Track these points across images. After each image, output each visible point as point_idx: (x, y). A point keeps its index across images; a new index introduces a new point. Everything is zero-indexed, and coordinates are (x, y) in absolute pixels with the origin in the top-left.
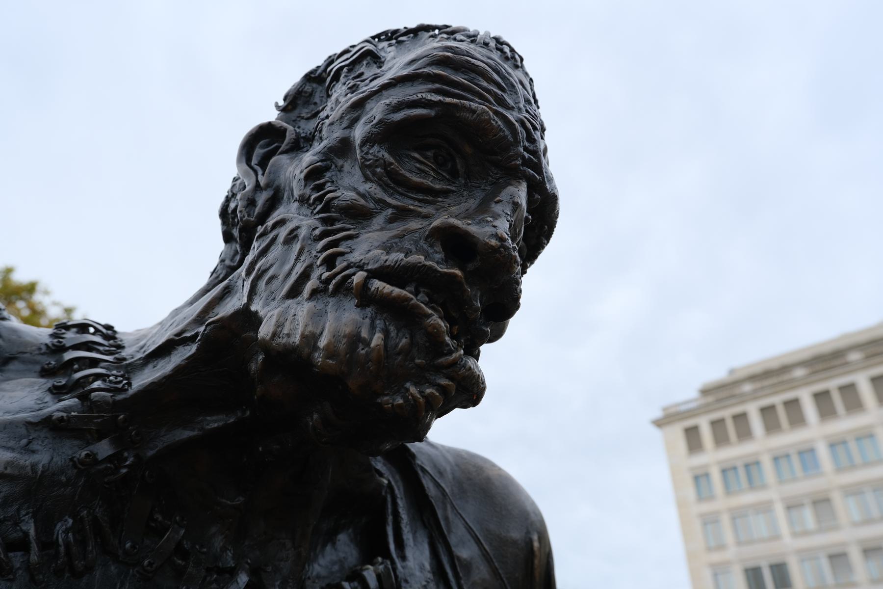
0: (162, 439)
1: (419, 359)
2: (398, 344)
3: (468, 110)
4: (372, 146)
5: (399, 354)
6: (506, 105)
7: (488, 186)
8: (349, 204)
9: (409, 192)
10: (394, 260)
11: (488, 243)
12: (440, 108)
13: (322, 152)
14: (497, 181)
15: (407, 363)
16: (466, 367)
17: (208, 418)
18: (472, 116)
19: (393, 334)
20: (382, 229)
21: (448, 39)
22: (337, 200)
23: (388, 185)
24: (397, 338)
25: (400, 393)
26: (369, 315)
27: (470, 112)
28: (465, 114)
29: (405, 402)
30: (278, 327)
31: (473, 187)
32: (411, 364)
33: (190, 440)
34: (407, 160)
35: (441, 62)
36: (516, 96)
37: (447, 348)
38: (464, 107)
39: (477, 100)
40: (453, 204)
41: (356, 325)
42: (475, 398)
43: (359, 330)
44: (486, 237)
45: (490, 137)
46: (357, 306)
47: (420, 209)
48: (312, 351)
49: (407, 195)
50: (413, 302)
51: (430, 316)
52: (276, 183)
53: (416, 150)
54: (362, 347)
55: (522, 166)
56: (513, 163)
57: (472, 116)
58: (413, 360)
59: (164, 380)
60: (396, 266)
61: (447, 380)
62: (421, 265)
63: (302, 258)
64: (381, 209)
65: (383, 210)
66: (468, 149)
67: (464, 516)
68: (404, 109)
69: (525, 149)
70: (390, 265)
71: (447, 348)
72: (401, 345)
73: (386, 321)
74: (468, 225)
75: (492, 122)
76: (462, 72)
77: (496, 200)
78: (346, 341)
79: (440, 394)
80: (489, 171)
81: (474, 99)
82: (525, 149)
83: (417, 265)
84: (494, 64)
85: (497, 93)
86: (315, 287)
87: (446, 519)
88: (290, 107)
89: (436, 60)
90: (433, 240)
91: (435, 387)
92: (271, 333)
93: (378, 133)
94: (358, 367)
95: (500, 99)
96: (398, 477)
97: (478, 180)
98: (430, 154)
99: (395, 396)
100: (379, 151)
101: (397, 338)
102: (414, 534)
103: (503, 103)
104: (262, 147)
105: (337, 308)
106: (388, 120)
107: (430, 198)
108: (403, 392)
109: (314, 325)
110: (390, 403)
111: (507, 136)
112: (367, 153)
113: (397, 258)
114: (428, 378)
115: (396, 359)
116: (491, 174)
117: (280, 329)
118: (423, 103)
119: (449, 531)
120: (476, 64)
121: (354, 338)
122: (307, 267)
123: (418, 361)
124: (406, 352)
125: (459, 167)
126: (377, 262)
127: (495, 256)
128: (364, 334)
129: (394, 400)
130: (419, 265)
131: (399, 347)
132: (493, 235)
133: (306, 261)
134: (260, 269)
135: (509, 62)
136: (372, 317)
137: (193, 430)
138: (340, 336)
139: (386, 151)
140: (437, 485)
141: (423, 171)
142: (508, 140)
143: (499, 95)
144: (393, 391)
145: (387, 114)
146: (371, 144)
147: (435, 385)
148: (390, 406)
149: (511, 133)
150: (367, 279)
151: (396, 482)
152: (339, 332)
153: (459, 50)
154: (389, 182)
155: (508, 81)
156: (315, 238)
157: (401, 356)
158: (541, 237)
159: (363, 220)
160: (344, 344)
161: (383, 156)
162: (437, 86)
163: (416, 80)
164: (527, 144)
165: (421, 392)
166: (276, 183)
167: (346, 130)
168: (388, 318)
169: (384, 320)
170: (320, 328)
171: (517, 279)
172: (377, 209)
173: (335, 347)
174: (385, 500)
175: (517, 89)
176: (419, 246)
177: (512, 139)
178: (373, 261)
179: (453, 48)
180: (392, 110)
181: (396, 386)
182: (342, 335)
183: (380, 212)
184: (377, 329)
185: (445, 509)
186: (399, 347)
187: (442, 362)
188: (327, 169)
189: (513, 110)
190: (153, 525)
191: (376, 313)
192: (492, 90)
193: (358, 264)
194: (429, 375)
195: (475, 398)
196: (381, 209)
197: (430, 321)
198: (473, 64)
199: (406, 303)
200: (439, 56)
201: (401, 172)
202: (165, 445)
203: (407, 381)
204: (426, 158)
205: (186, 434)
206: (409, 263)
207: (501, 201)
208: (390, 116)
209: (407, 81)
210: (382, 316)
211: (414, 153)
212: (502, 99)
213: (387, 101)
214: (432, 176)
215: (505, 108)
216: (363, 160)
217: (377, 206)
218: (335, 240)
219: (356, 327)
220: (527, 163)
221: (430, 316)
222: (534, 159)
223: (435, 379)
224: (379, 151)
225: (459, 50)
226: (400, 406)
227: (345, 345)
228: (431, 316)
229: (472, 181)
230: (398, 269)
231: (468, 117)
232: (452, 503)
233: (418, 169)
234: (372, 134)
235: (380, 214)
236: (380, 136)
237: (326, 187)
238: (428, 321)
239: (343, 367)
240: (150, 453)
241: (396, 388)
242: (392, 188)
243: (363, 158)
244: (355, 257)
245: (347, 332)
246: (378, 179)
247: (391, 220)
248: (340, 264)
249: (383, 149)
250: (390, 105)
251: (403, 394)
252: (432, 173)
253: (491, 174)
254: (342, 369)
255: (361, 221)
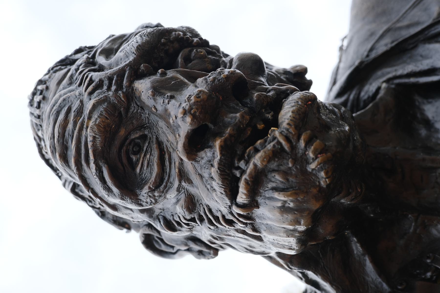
0: (374, 280)
1: (288, 164)
2: (280, 181)
3: (95, 142)
4: (141, 200)
5: (288, 180)
6: (81, 107)
7: (145, 111)
8: (186, 211)
9: (166, 172)
10: (220, 188)
11: (190, 123)
12: (100, 162)
13: (154, 222)
14: (140, 106)
15: (294, 172)
16: (288, 128)
17: (355, 252)
18: (98, 138)
19: (274, 185)
20: (198, 188)
21: (44, 140)
22: (185, 217)
23: (166, 187)
24: (276, 182)
25: (317, 174)
26: (263, 200)
27: (95, 140)
28: (98, 144)
29: (322, 170)
30: (284, 247)
31: (149, 122)
32: (293, 169)
33: (373, 261)
34: (144, 174)
35: (65, 159)
36: (71, 98)
37: (277, 146)
38: (94, 146)
39: (84, 134)
40: (167, 138)
41: (273, 209)
42: (310, 103)
43: (276, 207)
44: (186, 125)
45: (109, 122)
46: (258, 208)
47: (177, 164)
48: (297, 231)
49: (169, 173)
50: (248, 178)
51: (255, 165)
52: (183, 240)
53: (134, 169)
54: (288, 204)
55: (123, 89)
56: (123, 99)
57: (98, 138)
58: (290, 168)
59: (334, 287)
60: (223, 187)
61: (300, 141)
62: (218, 171)
63: (233, 234)
64: (184, 189)
65: (184, 188)
66: (122, 132)
67: (404, 11)
68: (108, 186)
69: (109, 89)
70: (224, 191)
71: (277, 146)
72: (281, 179)
73: (265, 190)
74: (180, 136)
75: (97, 123)
76: (67, 143)
77: (155, 111)
78: (286, 214)
79: (312, 145)
80: (134, 112)
81: (85, 136)
82: (109, 89)
83: (219, 174)
84: (53, 116)
85: (74, 116)
86: (251, 230)
87: (409, 26)
88: (127, 226)
89: (65, 164)
90: (198, 158)
91: (307, 149)
92: (289, 250)
93: (131, 198)
94: (303, 205)
95: (77, 113)
96: (379, 73)
97: (143, 120)
98: (134, 158)
99: (320, 177)
100: (143, 196)
101: (276, 182)
102: (424, 57)
103: (80, 110)
104: (160, 245)
105: (263, 219)
106: (119, 195)
107: (167, 156)
108: (316, 172)
109: (278, 232)
110: (325, 180)
111: (104, 108)
112: (147, 203)
113: (217, 187)
114: (301, 155)
115: (292, 181)
116: (135, 111)
117: (286, 246)
118: (99, 174)
119: (417, 24)
120: (58, 135)
121: (282, 210)
122: (238, 232)
123: (290, 165)
124: (286, 174)
125: (137, 135)
126: (224, 199)
127: (199, 115)
128: (279, 204)
129: (323, 178)
130: (219, 172)
131: (283, 180)
132: (183, 120)
133: (233, 232)
134: (245, 251)
135: (46, 95)
136: (265, 199)
137: (365, 260)
138: (283, 219)
139: (142, 191)
140: (382, 36)
141: (148, 164)
142: (107, 107)
143: (75, 114)
144: (316, 179)
145: (115, 196)
146: (139, 201)
147: (306, 149)
148: (327, 180)
149: (101, 105)
150: (238, 206)
151: (383, 75)
152: (280, 219)
153: (51, 146)
154: (163, 186)
155: (62, 104)
156: (216, 228)
157: (289, 178)
158: (171, 40)
159: (195, 199)
160: (288, 216)
161: (145, 193)
162: (83, 162)
163: (84, 176)
164: (105, 88)
165: (314, 160)
166: (183, 240)
167: (134, 211)
168: (263, 189)
169: (265, 191)
170: (281, 229)
171: (211, 82)
172: (185, 191)
173: (291, 221)
174: (398, 85)
175: (66, 97)
176: (204, 166)
177: (106, 104)
178: (223, 201)
179: (52, 152)
180: (111, 193)
181: (312, 178)
182: (282, 217)
183: (186, 189)
184: (272, 196)
185: (400, 28)
186: (283, 180)
187: (288, 148)
188: (165, 218)
189: (82, 100)
190: (435, 277)
191: (261, 196)
192: (73, 120)
193: (228, 209)
194: (299, 154)
195: (310, 103)
196: (184, 189)
197: (259, 164)
198: (59, 136)
199: (249, 183)
200: (61, 162)
201: (154, 181)
202: (378, 277)
203: (307, 170)
204: (138, 160)
205: (369, 266)
206: (219, 179)
207: (155, 107)
208: (117, 195)
209: (87, 182)
210: (262, 192)
211: (137, 171)
212: (77, 111)
213: (106, 196)
214: (150, 157)
215: (83, 108)
216: (152, 204)
217: (182, 192)
218: (214, 219)
219: (274, 209)
220: (120, 86)
221: (255, 165)
222: (115, 79)
223: (301, 149)
224: (143, 196)
225: (51, 146)
226: (326, 173)
227: (289, 215)
228: (255, 163)
229: (145, 123)
230: (225, 185)
231: (99, 141)
232: (395, 23)
233: (147, 167)
234: (132, 202)
235: (187, 189)
236: (132, 197)
237: (177, 220)
238: (259, 166)
239: (305, 215)
240: (385, 286)
241: (313, 177)
242: (167, 183)
243: (151, 205)
244: (225, 211)
245: (279, 215)
246: (163, 193)
247: (190, 181)
248: (230, 217)
249: (140, 194)
250: (108, 195)
251: (317, 172)
252: (148, 156)
253: (135, 111)
254: (306, 215)
255: (196, 200)
